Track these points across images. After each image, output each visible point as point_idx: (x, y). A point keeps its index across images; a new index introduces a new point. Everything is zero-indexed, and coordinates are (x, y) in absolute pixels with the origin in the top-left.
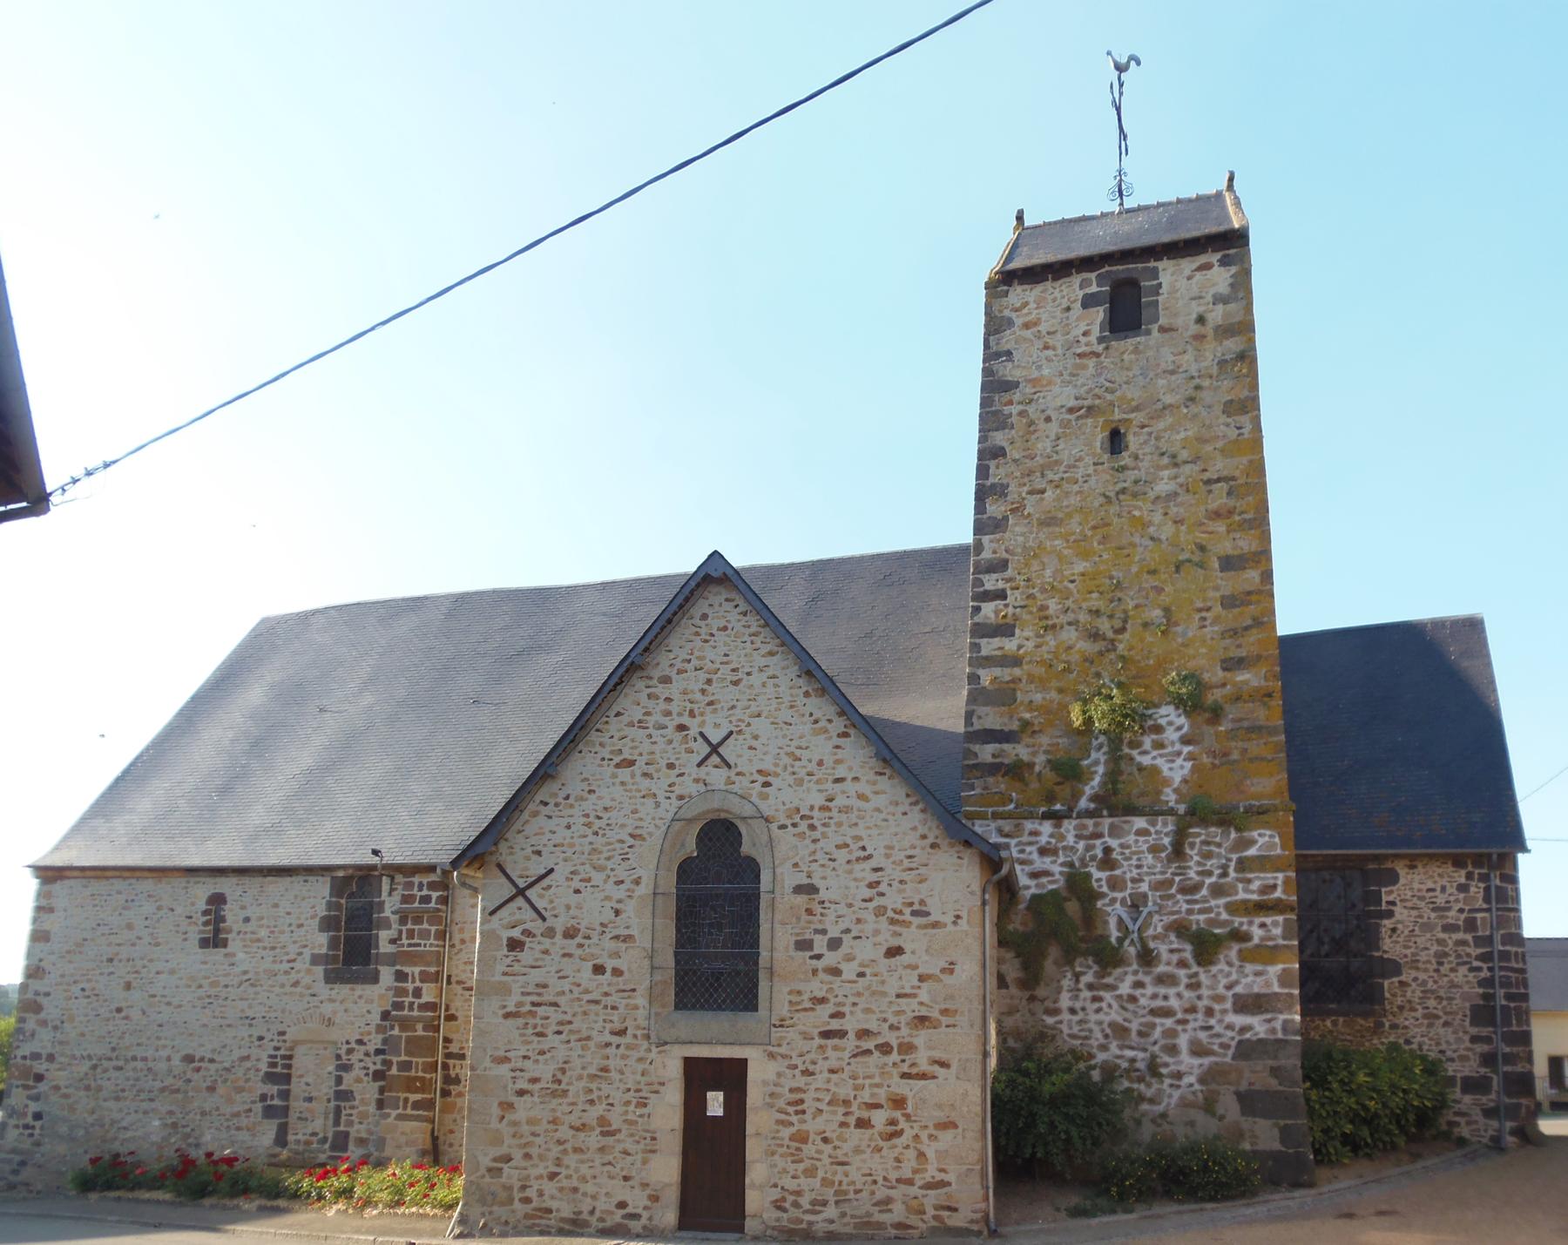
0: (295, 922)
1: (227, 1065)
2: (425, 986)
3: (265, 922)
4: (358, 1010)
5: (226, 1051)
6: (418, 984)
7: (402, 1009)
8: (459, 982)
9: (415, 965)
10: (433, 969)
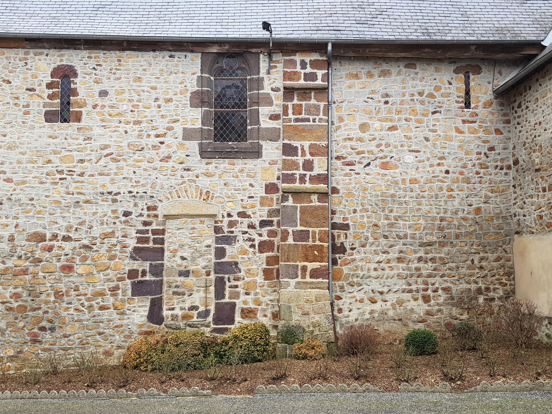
0: (162, 97)
1: (86, 242)
2: (316, 159)
3: (126, 95)
4: (242, 185)
5: (84, 228)
6: (308, 157)
7: (293, 181)
8: (338, 158)
9: (304, 139)
10: (324, 143)
